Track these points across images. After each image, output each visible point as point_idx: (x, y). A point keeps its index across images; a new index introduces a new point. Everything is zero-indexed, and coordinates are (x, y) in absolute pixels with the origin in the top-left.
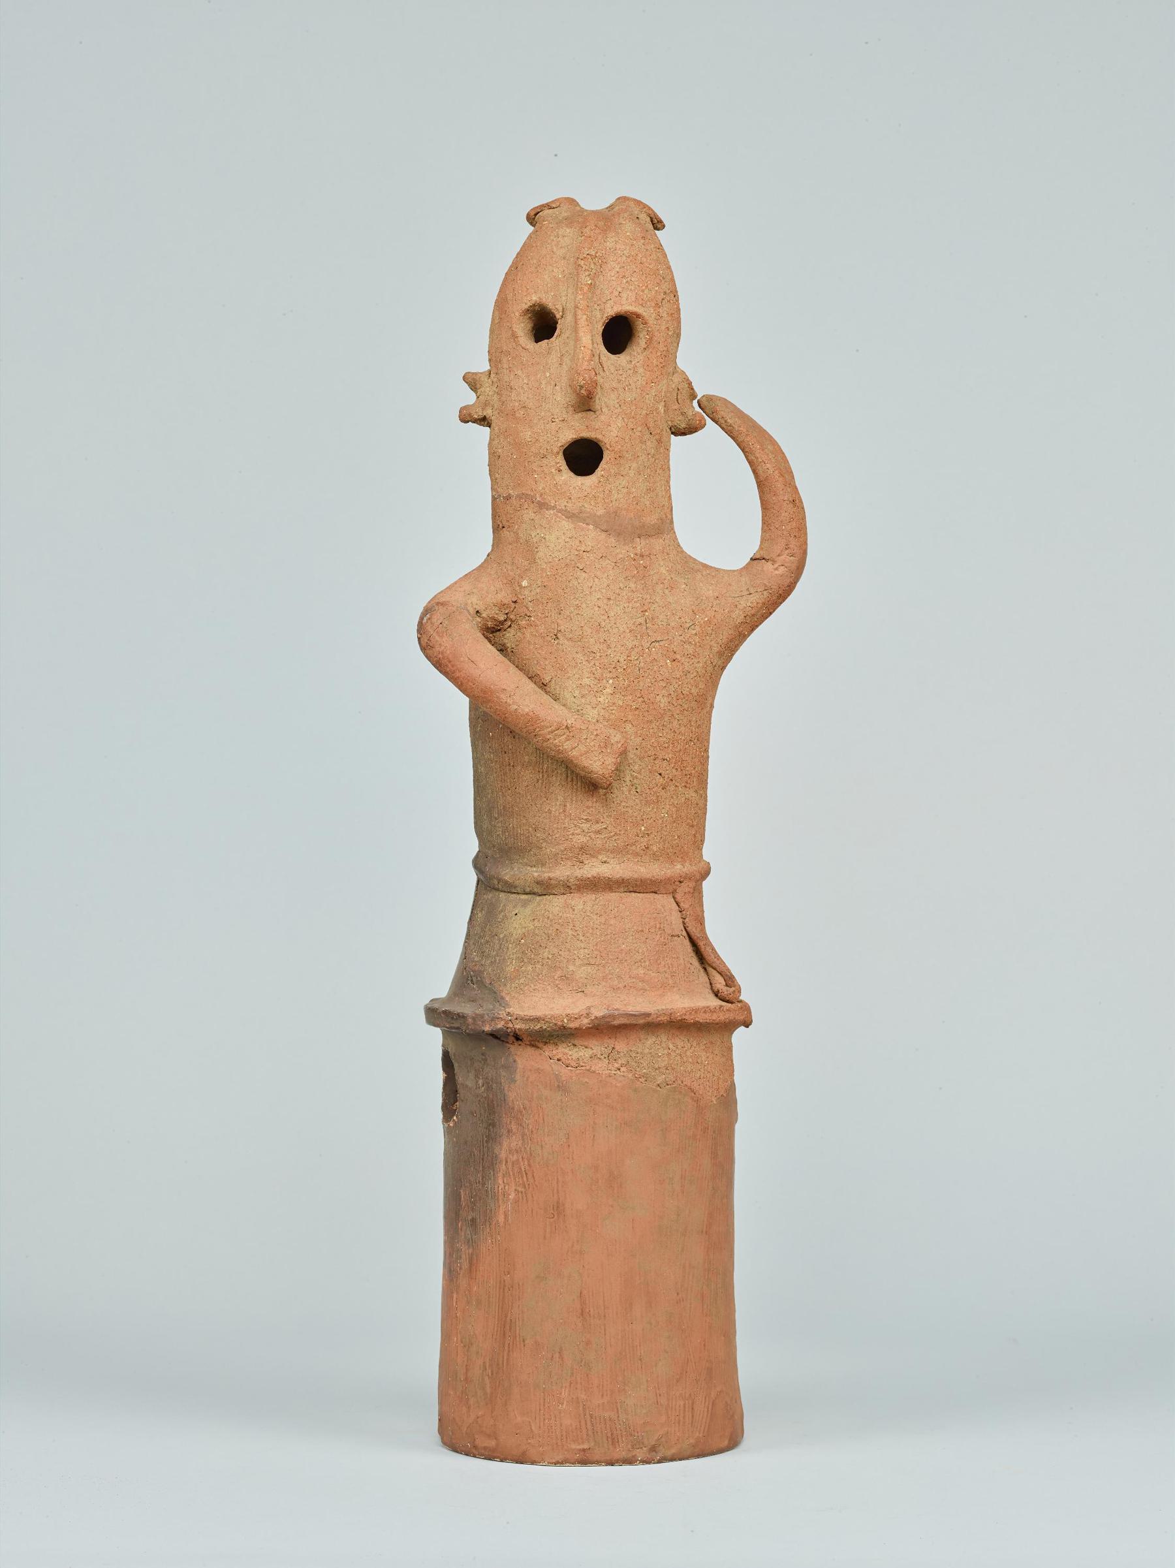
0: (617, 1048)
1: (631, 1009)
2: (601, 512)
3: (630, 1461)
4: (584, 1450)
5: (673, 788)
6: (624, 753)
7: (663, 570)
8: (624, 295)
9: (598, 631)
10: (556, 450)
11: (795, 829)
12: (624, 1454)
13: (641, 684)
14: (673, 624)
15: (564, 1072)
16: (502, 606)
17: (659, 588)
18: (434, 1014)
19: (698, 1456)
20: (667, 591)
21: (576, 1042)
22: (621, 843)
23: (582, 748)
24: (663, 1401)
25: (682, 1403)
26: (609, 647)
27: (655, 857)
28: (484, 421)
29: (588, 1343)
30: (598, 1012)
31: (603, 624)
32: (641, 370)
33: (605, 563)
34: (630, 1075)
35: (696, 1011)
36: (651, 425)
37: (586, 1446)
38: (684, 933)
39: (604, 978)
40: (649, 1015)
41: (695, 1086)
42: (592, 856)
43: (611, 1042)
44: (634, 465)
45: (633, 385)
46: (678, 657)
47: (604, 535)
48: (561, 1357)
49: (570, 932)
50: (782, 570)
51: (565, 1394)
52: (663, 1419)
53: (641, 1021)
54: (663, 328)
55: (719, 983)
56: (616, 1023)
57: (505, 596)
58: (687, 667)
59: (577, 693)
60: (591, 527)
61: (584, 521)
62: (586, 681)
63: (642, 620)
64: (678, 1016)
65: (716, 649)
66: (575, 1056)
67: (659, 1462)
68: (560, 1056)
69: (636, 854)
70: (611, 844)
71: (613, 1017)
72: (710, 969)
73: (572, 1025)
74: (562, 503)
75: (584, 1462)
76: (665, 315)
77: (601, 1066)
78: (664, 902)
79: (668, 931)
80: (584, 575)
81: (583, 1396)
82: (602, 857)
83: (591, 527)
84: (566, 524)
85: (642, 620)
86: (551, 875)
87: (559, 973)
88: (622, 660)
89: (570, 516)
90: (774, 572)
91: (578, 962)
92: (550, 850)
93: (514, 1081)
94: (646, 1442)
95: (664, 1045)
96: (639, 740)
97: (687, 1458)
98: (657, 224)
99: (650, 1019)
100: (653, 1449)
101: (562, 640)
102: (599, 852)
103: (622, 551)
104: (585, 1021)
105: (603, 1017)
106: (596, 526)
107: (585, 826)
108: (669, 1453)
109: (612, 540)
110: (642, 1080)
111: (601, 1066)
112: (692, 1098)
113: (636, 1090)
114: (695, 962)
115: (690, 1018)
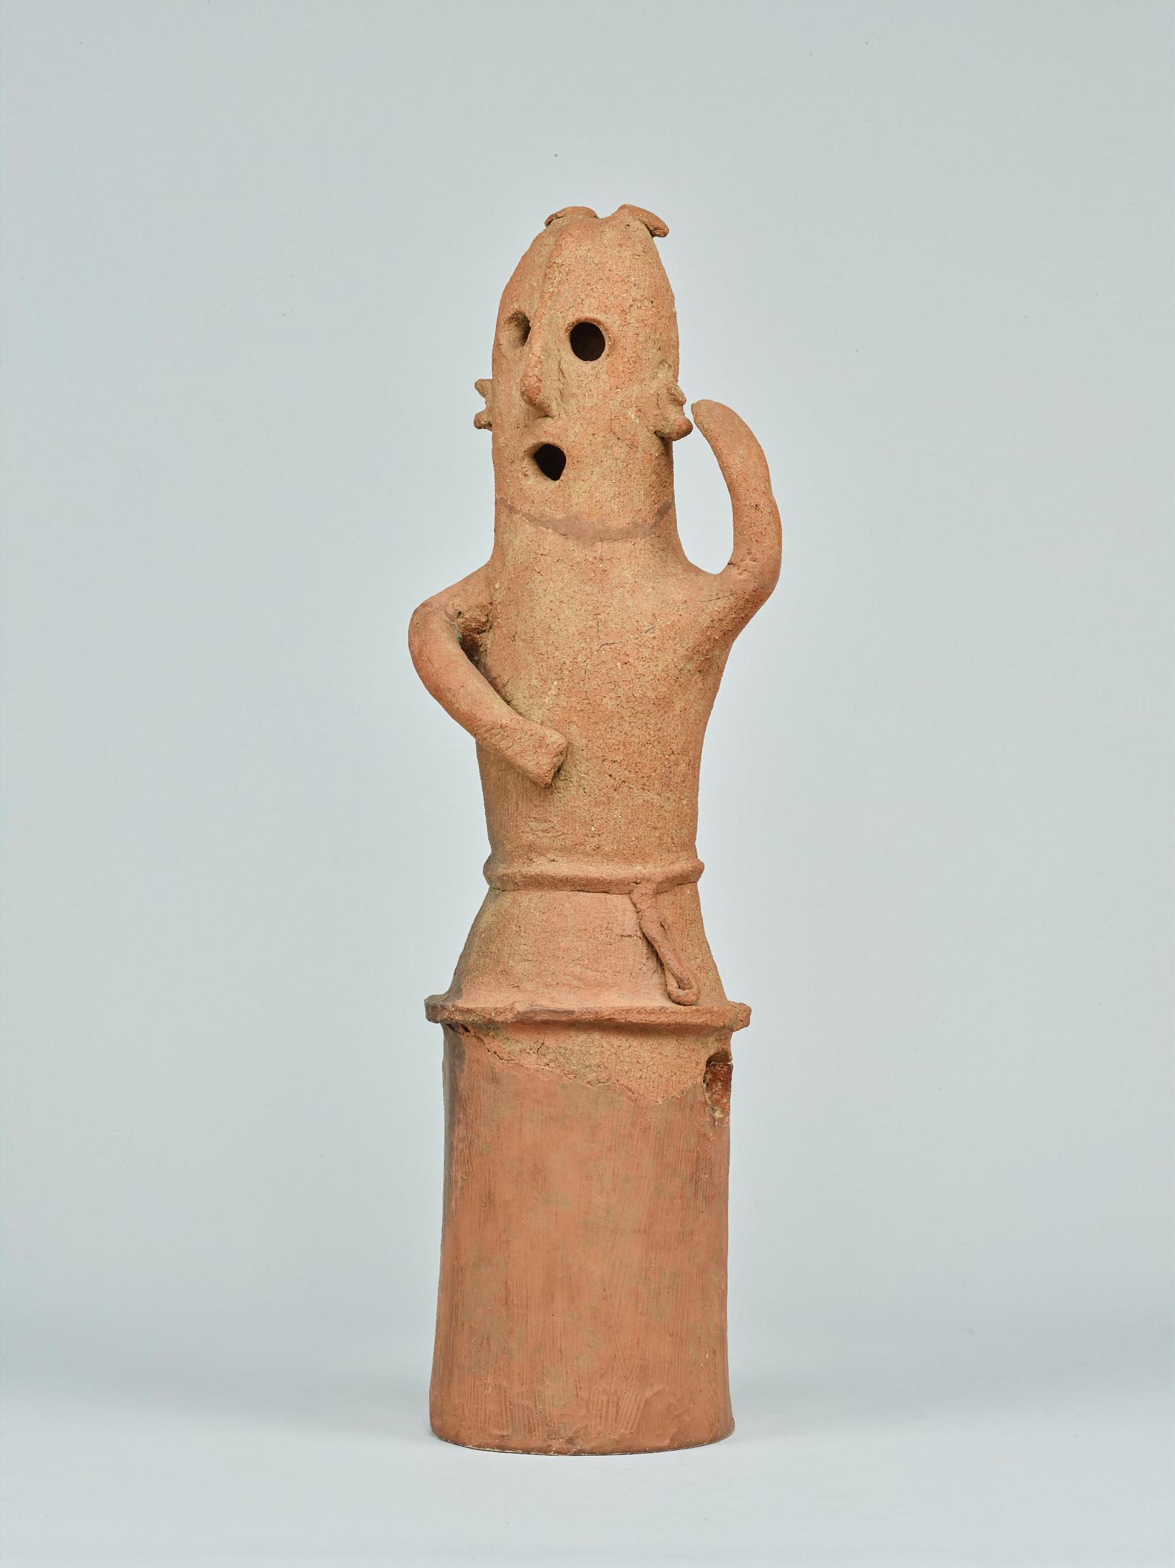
0: (547, 1043)
1: (557, 1006)
2: (560, 516)
3: (544, 1451)
4: (503, 1436)
5: (625, 790)
6: (566, 752)
7: (627, 574)
8: (587, 303)
9: (547, 634)
10: (522, 454)
11: (790, 841)
12: (539, 1444)
13: (587, 685)
14: (628, 627)
15: (498, 1064)
16: (482, 607)
17: (618, 592)
18: (434, 1010)
19: (624, 1452)
20: (627, 595)
21: (509, 1035)
22: (569, 843)
23: (517, 748)
24: (584, 1394)
25: (605, 1398)
26: (557, 649)
27: (608, 857)
28: (489, 426)
29: (511, 1331)
30: (520, 1008)
31: (553, 626)
32: (604, 376)
33: (561, 566)
34: (558, 1071)
35: (628, 1011)
36: (617, 429)
37: (505, 1433)
38: (639, 934)
39: (539, 975)
40: (572, 1012)
41: (634, 1085)
42: (541, 854)
43: (541, 1038)
44: (597, 470)
45: (594, 392)
46: (631, 660)
47: (562, 539)
48: (488, 1343)
49: (514, 928)
50: (745, 575)
51: (490, 1380)
52: (583, 1412)
53: (564, 1019)
54: (631, 334)
55: (673, 985)
56: (539, 1018)
57: (483, 599)
58: (641, 670)
59: (527, 694)
60: (550, 531)
61: (543, 524)
62: (534, 682)
63: (593, 623)
64: (606, 1015)
65: (681, 652)
66: (508, 1049)
67: (575, 1454)
68: (496, 1048)
69: (587, 854)
70: (558, 843)
71: (534, 1012)
72: (667, 973)
73: (498, 1019)
74: (527, 508)
75: (503, 1449)
76: (633, 321)
77: (530, 1061)
78: (619, 903)
79: (618, 931)
80: (540, 578)
81: (505, 1384)
82: (550, 856)
83: (550, 531)
84: (529, 528)
85: (593, 623)
86: (508, 872)
87: (501, 967)
88: (568, 662)
89: (532, 519)
90: (743, 579)
91: (517, 958)
92: (509, 847)
93: (462, 1071)
94: (562, 1432)
95: (597, 1043)
96: (584, 741)
97: (611, 1453)
98: (656, 230)
99: (574, 1017)
100: (570, 1441)
101: (519, 643)
102: (547, 850)
103: (579, 554)
104: (510, 1016)
105: (525, 1013)
106: (555, 530)
107: (533, 824)
108: (587, 1447)
109: (570, 544)
110: (572, 1076)
111: (530, 1061)
112: (629, 1098)
113: (564, 1087)
114: (652, 964)
115: (621, 1018)
